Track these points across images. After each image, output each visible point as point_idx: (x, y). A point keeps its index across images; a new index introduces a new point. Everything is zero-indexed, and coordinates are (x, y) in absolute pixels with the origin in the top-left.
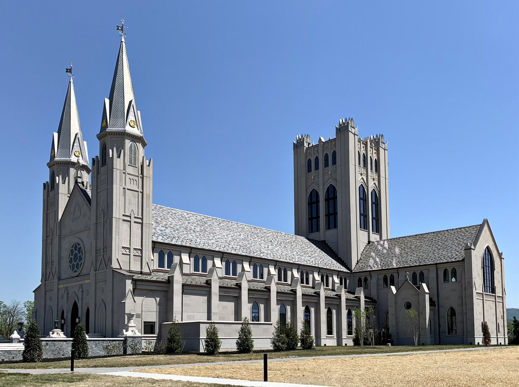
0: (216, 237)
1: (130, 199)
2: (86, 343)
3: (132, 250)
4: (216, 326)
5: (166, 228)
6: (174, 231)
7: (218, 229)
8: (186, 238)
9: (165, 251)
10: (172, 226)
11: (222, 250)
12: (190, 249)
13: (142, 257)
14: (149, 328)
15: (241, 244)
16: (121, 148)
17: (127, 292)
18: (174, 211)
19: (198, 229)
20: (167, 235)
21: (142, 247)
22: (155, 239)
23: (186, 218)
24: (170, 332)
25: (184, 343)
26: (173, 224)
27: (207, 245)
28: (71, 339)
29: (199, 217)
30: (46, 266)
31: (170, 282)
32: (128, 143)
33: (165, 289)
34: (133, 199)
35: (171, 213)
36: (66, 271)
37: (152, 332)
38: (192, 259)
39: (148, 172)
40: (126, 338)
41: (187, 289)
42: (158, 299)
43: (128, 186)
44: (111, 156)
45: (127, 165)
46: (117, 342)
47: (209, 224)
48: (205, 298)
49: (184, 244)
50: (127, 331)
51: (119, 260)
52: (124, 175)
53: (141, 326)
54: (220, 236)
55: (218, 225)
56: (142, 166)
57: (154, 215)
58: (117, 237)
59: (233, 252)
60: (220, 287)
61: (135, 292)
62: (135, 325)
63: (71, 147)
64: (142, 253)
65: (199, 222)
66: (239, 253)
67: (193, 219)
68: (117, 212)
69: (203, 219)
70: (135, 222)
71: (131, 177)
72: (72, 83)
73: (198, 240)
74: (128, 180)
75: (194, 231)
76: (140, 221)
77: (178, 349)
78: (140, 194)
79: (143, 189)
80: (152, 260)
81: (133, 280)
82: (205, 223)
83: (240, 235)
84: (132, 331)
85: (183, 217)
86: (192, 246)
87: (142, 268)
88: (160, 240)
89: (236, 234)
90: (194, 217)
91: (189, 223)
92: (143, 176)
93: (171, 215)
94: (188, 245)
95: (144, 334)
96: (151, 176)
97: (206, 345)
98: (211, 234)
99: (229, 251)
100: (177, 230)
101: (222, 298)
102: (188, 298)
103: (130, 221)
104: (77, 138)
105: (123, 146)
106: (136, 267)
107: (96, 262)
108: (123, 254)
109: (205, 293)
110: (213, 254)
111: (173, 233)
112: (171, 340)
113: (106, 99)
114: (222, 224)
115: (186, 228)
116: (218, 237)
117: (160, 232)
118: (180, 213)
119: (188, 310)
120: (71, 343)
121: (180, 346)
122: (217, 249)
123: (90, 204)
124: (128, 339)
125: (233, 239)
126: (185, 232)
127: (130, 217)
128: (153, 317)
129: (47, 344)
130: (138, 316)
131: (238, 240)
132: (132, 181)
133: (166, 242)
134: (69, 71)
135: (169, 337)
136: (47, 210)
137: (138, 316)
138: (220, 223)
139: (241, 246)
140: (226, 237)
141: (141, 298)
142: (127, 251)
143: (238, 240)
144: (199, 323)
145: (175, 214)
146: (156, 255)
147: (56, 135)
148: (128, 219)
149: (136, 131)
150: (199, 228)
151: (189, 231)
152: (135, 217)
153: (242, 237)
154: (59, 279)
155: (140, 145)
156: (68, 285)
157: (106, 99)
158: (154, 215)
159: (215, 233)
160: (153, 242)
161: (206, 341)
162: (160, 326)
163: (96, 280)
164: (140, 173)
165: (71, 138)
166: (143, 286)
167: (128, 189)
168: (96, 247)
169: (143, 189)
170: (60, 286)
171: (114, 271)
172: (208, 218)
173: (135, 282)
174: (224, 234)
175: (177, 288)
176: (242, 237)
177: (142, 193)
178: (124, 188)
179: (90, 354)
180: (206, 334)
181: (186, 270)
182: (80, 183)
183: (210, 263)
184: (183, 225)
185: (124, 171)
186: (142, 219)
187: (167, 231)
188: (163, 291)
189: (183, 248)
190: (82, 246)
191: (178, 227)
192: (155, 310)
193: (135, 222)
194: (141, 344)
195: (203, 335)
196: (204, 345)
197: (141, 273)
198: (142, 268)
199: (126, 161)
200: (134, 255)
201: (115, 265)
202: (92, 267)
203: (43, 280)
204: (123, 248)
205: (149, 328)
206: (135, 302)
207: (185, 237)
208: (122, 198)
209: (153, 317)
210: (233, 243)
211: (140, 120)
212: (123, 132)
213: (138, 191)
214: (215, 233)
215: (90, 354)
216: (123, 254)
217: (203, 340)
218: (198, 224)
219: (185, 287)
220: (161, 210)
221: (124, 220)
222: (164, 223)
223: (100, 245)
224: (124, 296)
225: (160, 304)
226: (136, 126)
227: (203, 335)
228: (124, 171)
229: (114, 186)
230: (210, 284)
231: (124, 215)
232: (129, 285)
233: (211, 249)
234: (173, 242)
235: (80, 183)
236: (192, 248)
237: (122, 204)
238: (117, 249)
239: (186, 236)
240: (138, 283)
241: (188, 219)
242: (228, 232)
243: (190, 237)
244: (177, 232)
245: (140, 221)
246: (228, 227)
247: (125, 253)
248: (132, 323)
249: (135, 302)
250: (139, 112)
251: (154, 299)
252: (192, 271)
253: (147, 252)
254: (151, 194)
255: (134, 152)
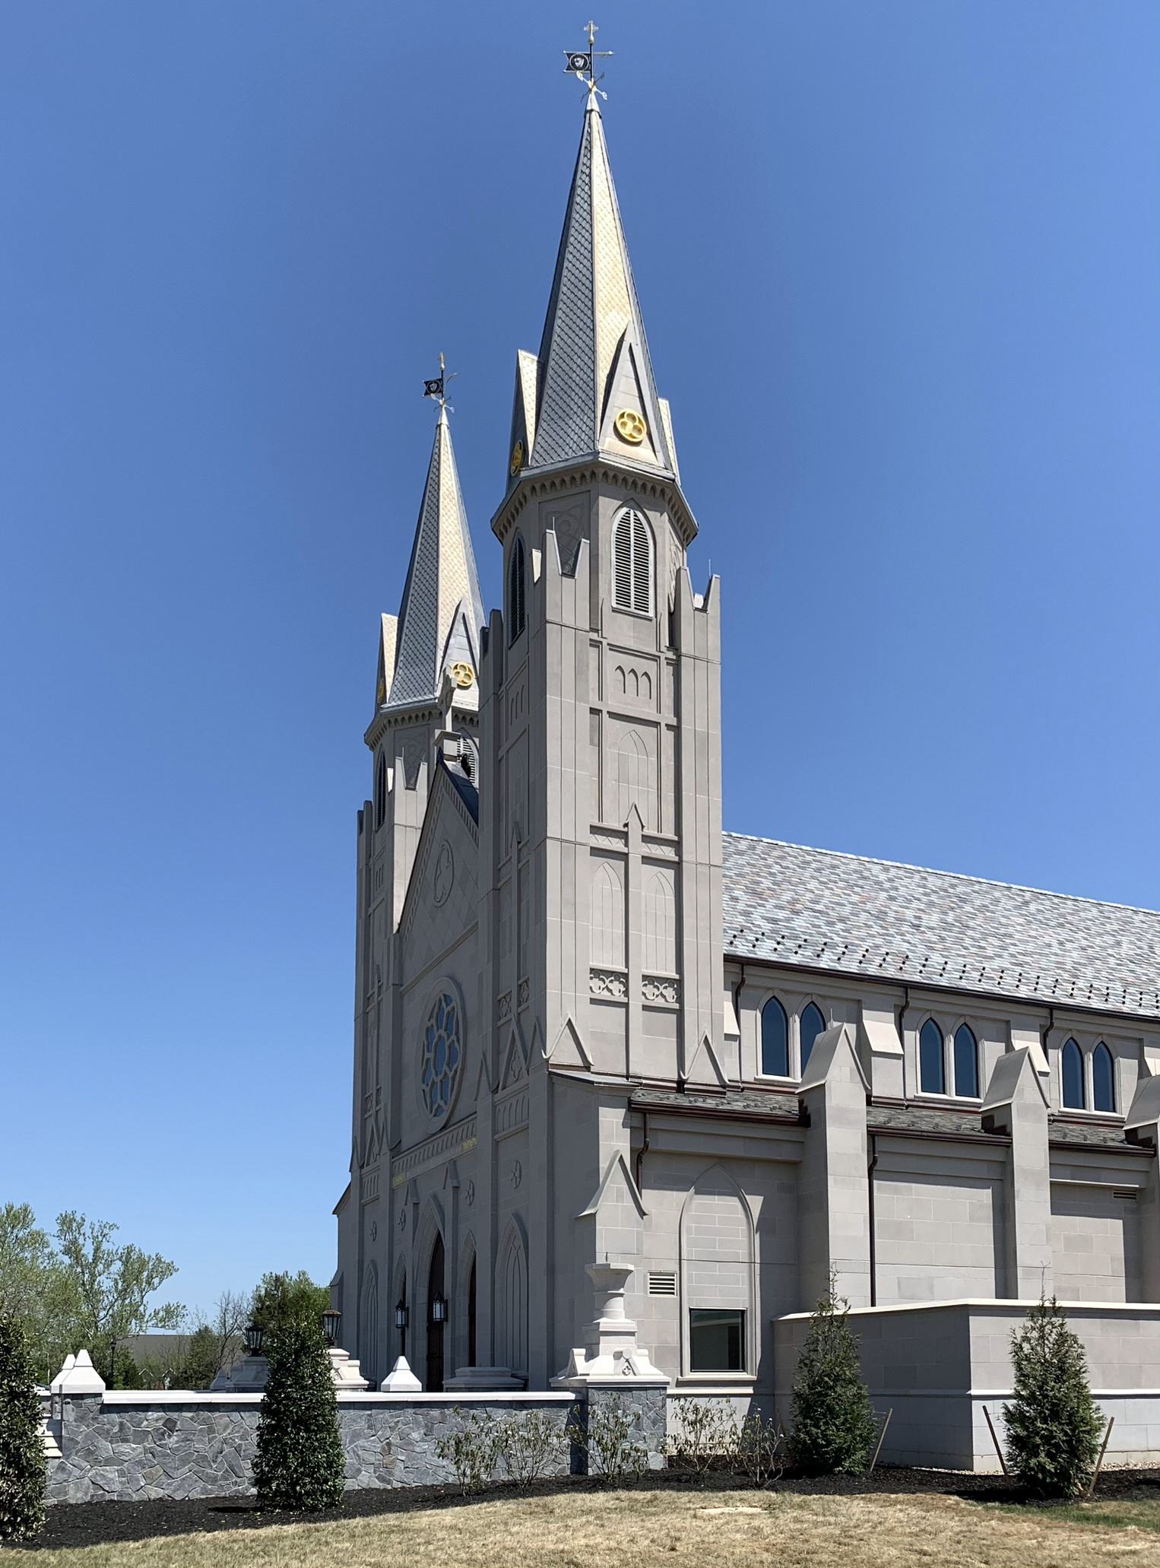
0: (1012, 949)
1: (622, 760)
2: (329, 1427)
3: (635, 983)
4: (1072, 1325)
5: (797, 913)
6: (830, 924)
7: (1021, 920)
8: (883, 951)
9: (792, 999)
10: (818, 907)
11: (1044, 994)
12: (900, 992)
13: (680, 1013)
14: (715, 1339)
15: (1126, 975)
16: (578, 529)
17: (603, 1165)
18: (827, 859)
19: (933, 919)
20: (796, 938)
21: (680, 968)
22: (742, 949)
23: (877, 883)
24: (806, 1363)
25: (880, 1420)
26: (825, 901)
27: (976, 975)
28: (257, 1397)
29: (933, 882)
30: (364, 1110)
31: (807, 1118)
32: (610, 514)
33: (786, 1153)
34: (635, 758)
35: (814, 865)
36: (417, 1122)
37: (736, 1362)
38: (912, 1037)
39: (704, 636)
40: (585, 1394)
41: (893, 1148)
42: (756, 1202)
43: (612, 702)
44: (537, 575)
45: (607, 611)
46: (541, 1413)
47: (978, 903)
48: (985, 1196)
49: (872, 970)
50: (591, 1355)
51: (582, 1026)
52: (593, 652)
53: (677, 1333)
54: (1030, 948)
55: (1017, 907)
56: (674, 617)
57: (747, 869)
58: (568, 922)
59: (1096, 1004)
60: (1054, 1146)
61: (645, 1167)
62: (629, 1325)
63: (440, 654)
64: (680, 999)
65: (934, 898)
66: (1125, 1009)
67: (908, 886)
68: (567, 814)
69: (953, 886)
70: (647, 860)
71: (628, 662)
72: (444, 428)
73: (936, 959)
74: (611, 677)
75: (917, 927)
76: (669, 853)
77: (849, 1452)
78: (668, 737)
79: (678, 713)
80: (729, 1037)
81: (632, 1108)
82: (964, 901)
83: (1119, 943)
84: (618, 1356)
85: (865, 878)
86: (907, 977)
87: (681, 1065)
88: (765, 952)
89: (1098, 941)
90: (909, 884)
91: (892, 898)
92: (679, 656)
93: (818, 870)
94: (891, 972)
95: (694, 1367)
96: (715, 655)
97: (1015, 1440)
98: (991, 940)
99: (1079, 1000)
100: (842, 920)
101: (1066, 1199)
102: (903, 1200)
103: (624, 857)
104: (459, 617)
105: (589, 529)
106: (654, 1062)
107: (497, 1052)
108: (593, 1001)
109: (983, 1171)
110: (1006, 1011)
111: (825, 929)
112: (814, 1404)
113: (522, 354)
114: (1033, 907)
115: (881, 916)
116: (1021, 948)
117: (767, 927)
118: (854, 865)
119: (903, 1250)
120: (255, 1419)
121: (866, 1440)
122: (1024, 992)
123: (476, 821)
124: (595, 1396)
125: (1091, 960)
126: (876, 929)
127: (624, 836)
128: (732, 1285)
129: (170, 1425)
130: (662, 1284)
131: (1112, 960)
132: (630, 678)
133: (794, 960)
134: (434, 387)
135: (801, 1387)
136: (368, 905)
137: (662, 1284)
138: (1026, 903)
139: (1126, 984)
140: (1056, 949)
141: (676, 1197)
142: (616, 987)
143: (1112, 961)
144: (964, 1312)
145: (834, 867)
146: (752, 1019)
147: (390, 623)
148: (617, 845)
149: (645, 458)
150: (935, 917)
151: (893, 925)
152: (646, 839)
153: (1125, 949)
154: (396, 1150)
155: (662, 522)
156: (418, 1170)
157: (522, 354)
158: (747, 869)
159: (1011, 936)
160: (729, 959)
161: (1011, 1417)
162: (770, 1328)
163: (495, 1132)
164: (665, 641)
165: (440, 621)
166: (684, 1137)
167: (613, 715)
168: (496, 990)
169: (678, 713)
170: (399, 1179)
171: (555, 1078)
172: (971, 883)
173: (641, 1116)
174: (1047, 940)
175: (845, 1142)
176: (1125, 949)
177: (677, 729)
178: (593, 711)
179: (360, 1478)
180: (1012, 1372)
181: (889, 1082)
182: (453, 758)
183: (991, 1053)
184: (869, 906)
185: (594, 636)
186: (677, 845)
187: (800, 923)
188: (764, 1150)
189: (866, 986)
190: (456, 1002)
191: (847, 910)
192: (743, 1253)
193: (647, 860)
194: (660, 1420)
195: (993, 1378)
196: (1002, 1435)
197: (681, 1086)
198: (681, 1065)
199: (602, 593)
200: (645, 1008)
201: (558, 1051)
202: (484, 1078)
203: (356, 1167)
204: (596, 973)
205: (715, 1339)
206: (642, 1214)
207: (877, 947)
208: (589, 755)
209: (732, 1285)
210: (1089, 972)
211: (669, 433)
212: (585, 465)
213: (656, 724)
214: (1011, 936)
215: (360, 1478)
216: (593, 1001)
217: (996, 1409)
218: (931, 904)
219: (881, 1144)
220: (775, 853)
221: (596, 852)
222: (787, 896)
223: (509, 983)
224: (591, 1186)
225: (765, 1227)
226: (646, 441)
227: (993, 1378)
228: (594, 636)
229: (551, 698)
230: (1005, 1131)
231: (595, 830)
232: (614, 1135)
233: (997, 990)
234: (825, 962)
235: (453, 758)
236: (907, 986)
237: (590, 777)
238: (568, 982)
239: (879, 941)
240: (654, 1122)
241: (887, 885)
242: (1064, 934)
243: (899, 945)
244: (840, 926)
245: (669, 853)
246: (1063, 916)
247: (605, 995)
248: (616, 1315)
249: (642, 1214)
250: (664, 404)
251: (734, 1202)
252: (915, 1090)
253: (705, 992)
254: (716, 732)
255: (634, 553)
